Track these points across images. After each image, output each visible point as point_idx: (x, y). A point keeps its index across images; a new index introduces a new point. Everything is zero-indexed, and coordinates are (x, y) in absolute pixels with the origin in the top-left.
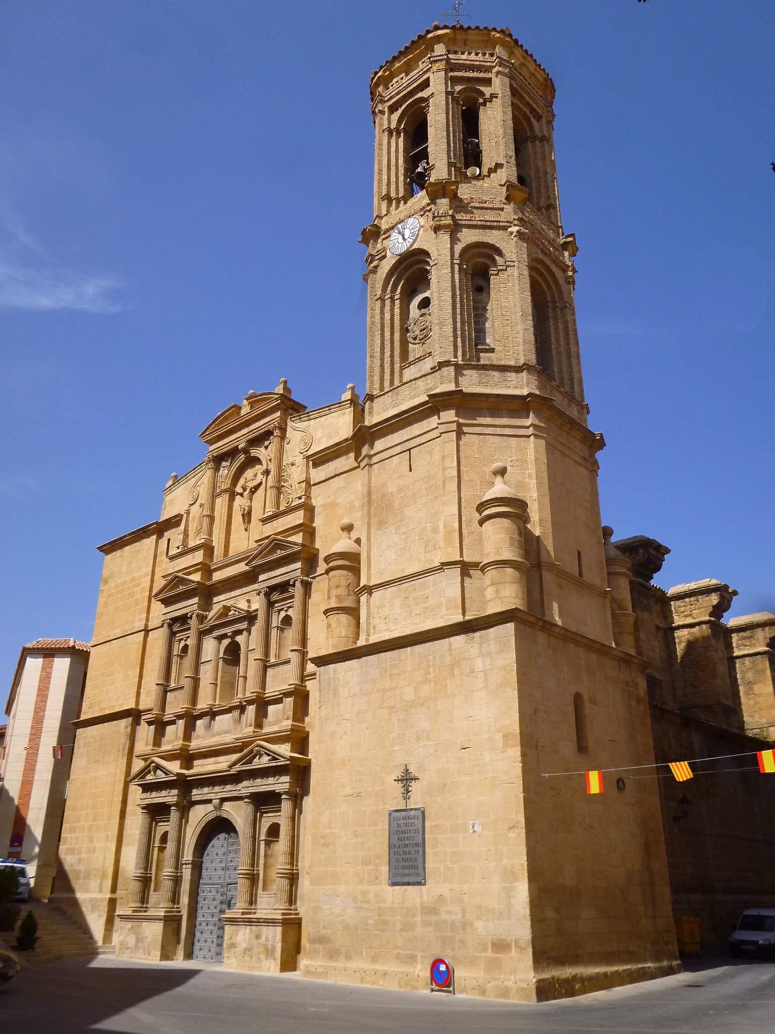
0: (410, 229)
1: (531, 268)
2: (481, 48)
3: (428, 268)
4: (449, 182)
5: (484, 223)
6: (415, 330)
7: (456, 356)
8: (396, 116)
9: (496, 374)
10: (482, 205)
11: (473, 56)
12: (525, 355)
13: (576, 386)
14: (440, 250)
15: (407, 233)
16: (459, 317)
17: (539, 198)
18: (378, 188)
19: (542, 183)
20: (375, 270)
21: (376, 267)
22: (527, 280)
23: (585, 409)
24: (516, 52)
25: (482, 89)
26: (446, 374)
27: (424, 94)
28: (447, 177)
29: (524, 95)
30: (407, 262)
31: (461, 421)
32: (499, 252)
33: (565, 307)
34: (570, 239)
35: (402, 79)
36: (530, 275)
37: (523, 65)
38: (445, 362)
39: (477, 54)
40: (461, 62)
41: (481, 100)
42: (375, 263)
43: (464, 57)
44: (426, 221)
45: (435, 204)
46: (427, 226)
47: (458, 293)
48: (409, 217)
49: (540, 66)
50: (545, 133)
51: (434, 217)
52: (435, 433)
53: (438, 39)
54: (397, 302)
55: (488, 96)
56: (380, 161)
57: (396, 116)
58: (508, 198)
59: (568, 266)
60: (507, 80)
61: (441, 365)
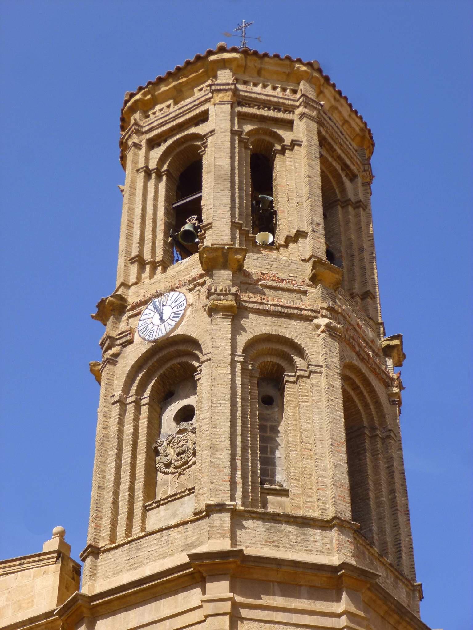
0: (171, 306)
1: (345, 378)
2: (280, 81)
3: (196, 364)
4: (232, 250)
5: (279, 309)
6: (169, 453)
7: (233, 498)
8: (157, 153)
9: (292, 529)
10: (278, 284)
11: (269, 90)
12: (335, 504)
13: (404, 556)
14: (217, 343)
15: (167, 312)
16: (239, 439)
17: (352, 280)
18: (126, 246)
19: (356, 262)
20: (114, 360)
21: (116, 355)
22: (339, 394)
23: (417, 591)
24: (326, 91)
25: (280, 132)
26: (217, 523)
27: (201, 129)
28: (229, 242)
29: (335, 146)
30: (164, 352)
31: (238, 599)
32: (300, 351)
33: (389, 437)
34: (395, 342)
35: (168, 106)
36: (343, 388)
37: (334, 108)
38: (218, 505)
39: (274, 88)
40: (253, 95)
41: (278, 147)
42: (114, 350)
43: (259, 89)
44: (197, 299)
45: (211, 276)
46: (199, 305)
47: (239, 404)
48: (172, 290)
49: (356, 112)
50: (361, 197)
51: (209, 295)
52: (197, 616)
53: (224, 64)
54: (145, 410)
55: (287, 142)
56: (131, 210)
57: (157, 153)
58: (314, 279)
59: (392, 379)
60: (314, 126)
61: (211, 510)
